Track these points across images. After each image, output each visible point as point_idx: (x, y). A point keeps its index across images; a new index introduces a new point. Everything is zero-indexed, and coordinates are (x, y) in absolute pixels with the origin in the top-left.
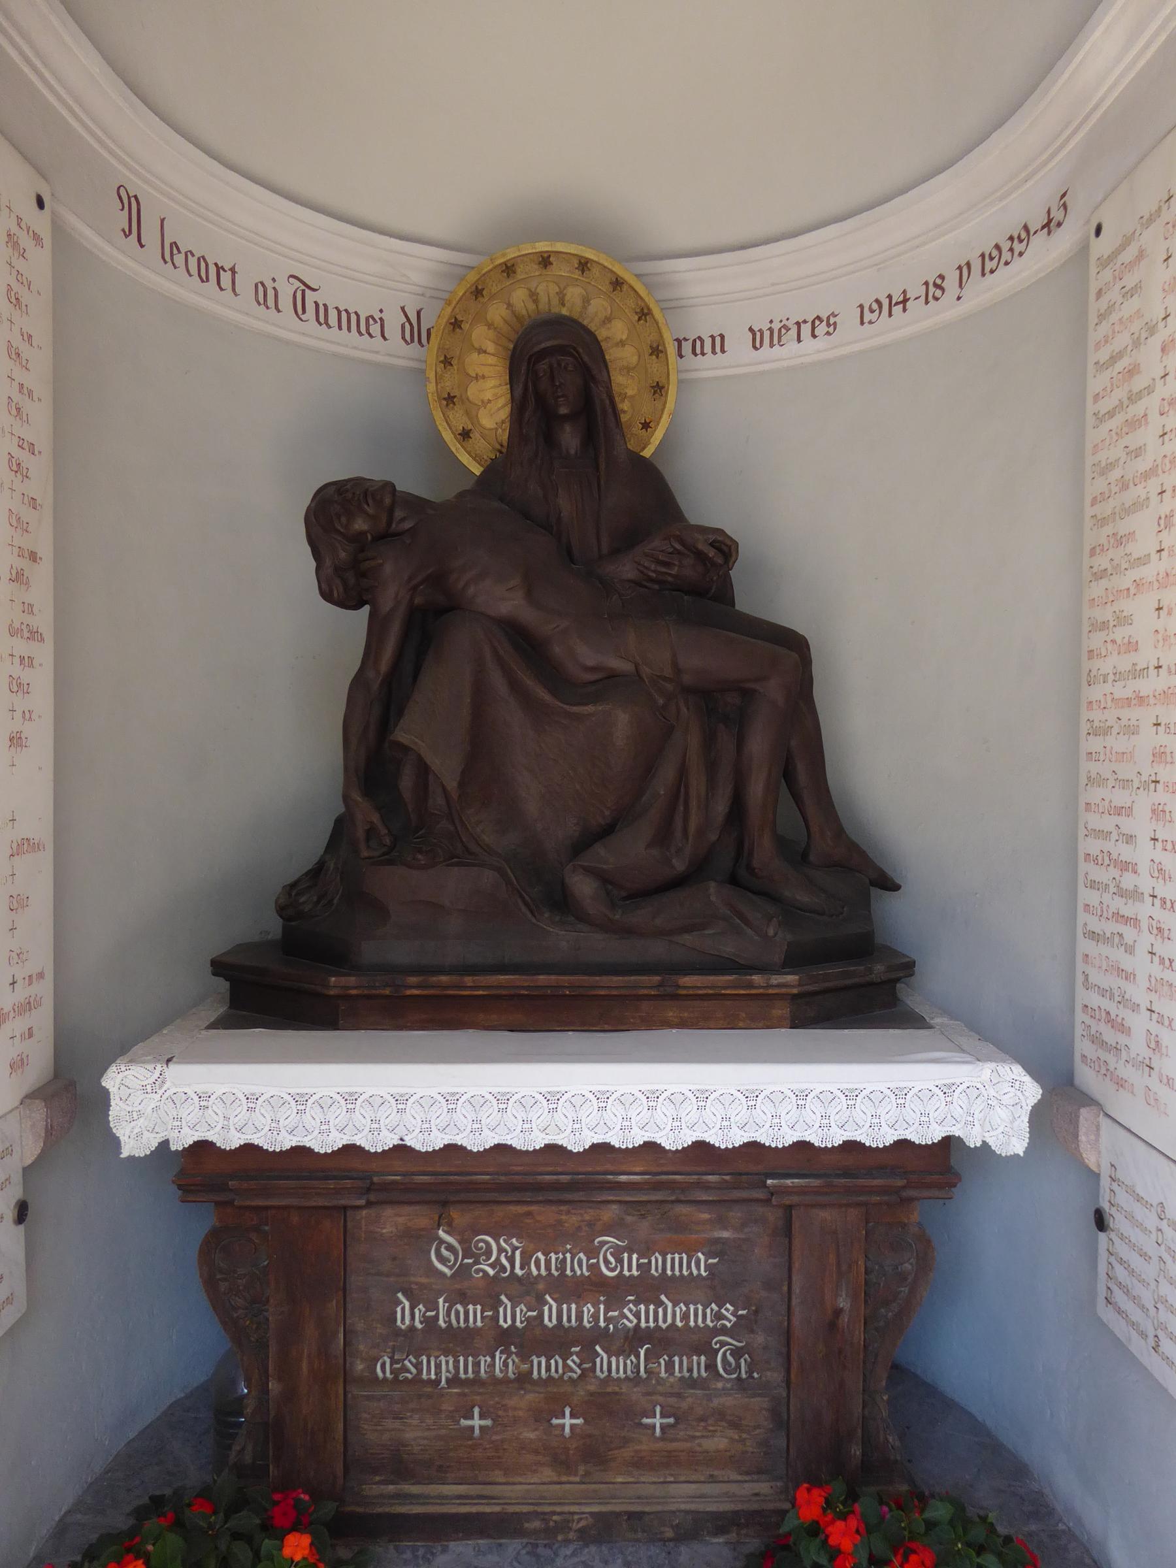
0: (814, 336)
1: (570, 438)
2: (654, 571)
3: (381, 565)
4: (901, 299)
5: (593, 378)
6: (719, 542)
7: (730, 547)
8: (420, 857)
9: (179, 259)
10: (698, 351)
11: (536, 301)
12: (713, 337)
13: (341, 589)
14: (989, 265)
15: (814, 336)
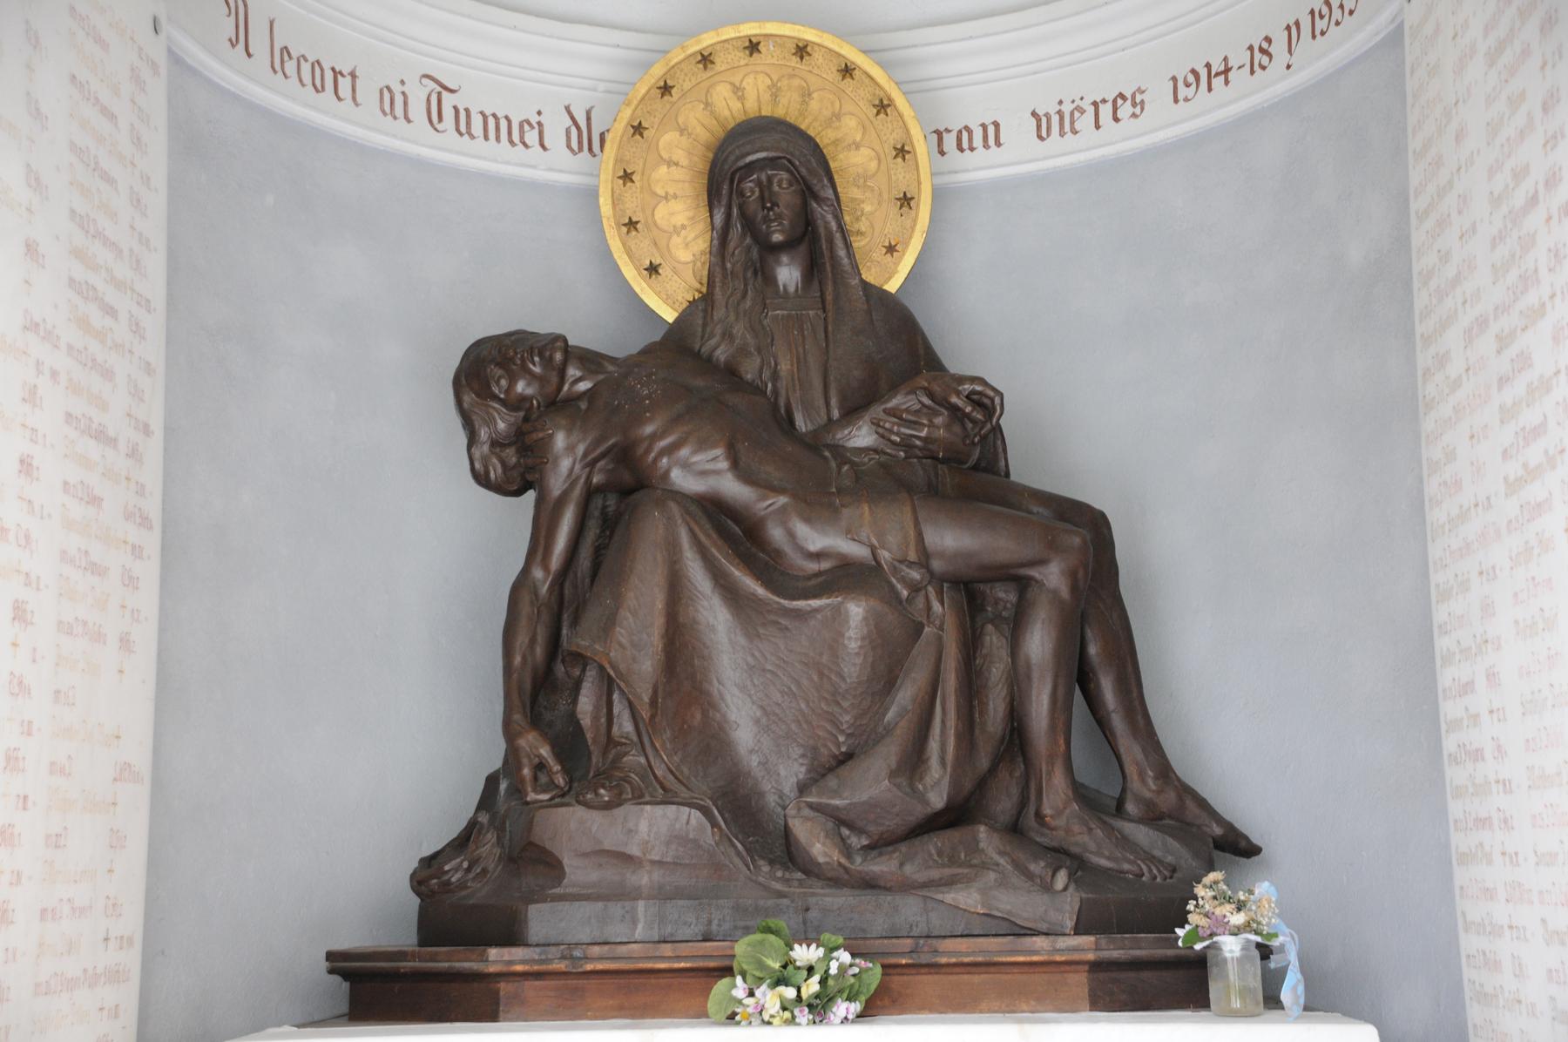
0: (1116, 119)
1: (788, 274)
2: (897, 434)
3: (551, 436)
4: (1222, 68)
5: (816, 197)
6: (979, 393)
7: (993, 400)
8: (602, 791)
9: (290, 67)
10: (965, 145)
11: (741, 99)
12: (984, 126)
13: (499, 470)
14: (1321, 25)
15: (1116, 119)
